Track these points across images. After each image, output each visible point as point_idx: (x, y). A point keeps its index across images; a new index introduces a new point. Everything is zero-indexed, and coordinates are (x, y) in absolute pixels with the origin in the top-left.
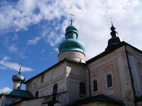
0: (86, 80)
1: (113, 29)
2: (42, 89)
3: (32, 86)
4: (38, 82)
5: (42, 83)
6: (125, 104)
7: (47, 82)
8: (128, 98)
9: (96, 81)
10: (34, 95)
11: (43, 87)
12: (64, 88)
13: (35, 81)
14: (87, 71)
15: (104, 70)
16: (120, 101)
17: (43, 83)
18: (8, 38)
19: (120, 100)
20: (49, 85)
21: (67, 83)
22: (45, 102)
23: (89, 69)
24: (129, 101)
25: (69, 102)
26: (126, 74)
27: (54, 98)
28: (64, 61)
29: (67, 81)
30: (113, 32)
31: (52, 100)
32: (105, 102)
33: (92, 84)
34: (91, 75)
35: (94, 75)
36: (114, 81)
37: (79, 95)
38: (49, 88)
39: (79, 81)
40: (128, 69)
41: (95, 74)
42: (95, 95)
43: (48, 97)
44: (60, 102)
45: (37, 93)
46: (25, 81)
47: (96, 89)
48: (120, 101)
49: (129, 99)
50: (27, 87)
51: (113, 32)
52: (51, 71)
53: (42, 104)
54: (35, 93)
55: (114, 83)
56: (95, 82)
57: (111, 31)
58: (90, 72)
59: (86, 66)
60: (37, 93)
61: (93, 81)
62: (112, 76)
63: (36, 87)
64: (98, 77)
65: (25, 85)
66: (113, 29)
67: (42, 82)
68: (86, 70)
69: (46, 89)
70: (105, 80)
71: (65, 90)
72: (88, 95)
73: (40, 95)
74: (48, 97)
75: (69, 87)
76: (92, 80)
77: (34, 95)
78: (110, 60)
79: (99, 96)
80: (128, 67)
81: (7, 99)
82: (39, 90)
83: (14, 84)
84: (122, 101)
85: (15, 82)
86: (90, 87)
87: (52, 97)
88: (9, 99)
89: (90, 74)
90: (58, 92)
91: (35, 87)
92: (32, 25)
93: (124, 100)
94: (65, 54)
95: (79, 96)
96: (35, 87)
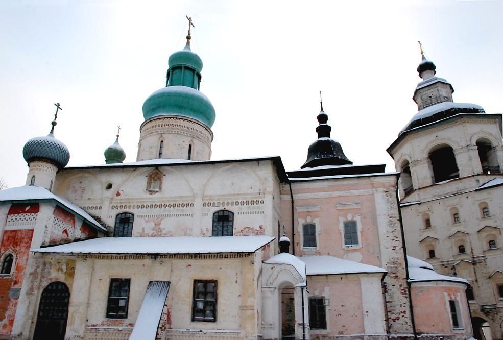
1: (323, 118)
6: (386, 283)
7: (181, 197)
14: (288, 197)
23: (295, 197)
24: (395, 278)
26: (392, 230)
30: (324, 130)
34: (298, 209)
35: (306, 210)
36: (362, 236)
40: (399, 221)
41: (310, 210)
46: (487, 234)
49: (397, 276)
51: (324, 130)
57: (317, 124)
62: (359, 227)
66: (323, 118)
76: (300, 224)
78: (355, 192)
80: (399, 218)
81: (56, 222)
85: (32, 164)
94: (169, 125)
96: (112, 199)
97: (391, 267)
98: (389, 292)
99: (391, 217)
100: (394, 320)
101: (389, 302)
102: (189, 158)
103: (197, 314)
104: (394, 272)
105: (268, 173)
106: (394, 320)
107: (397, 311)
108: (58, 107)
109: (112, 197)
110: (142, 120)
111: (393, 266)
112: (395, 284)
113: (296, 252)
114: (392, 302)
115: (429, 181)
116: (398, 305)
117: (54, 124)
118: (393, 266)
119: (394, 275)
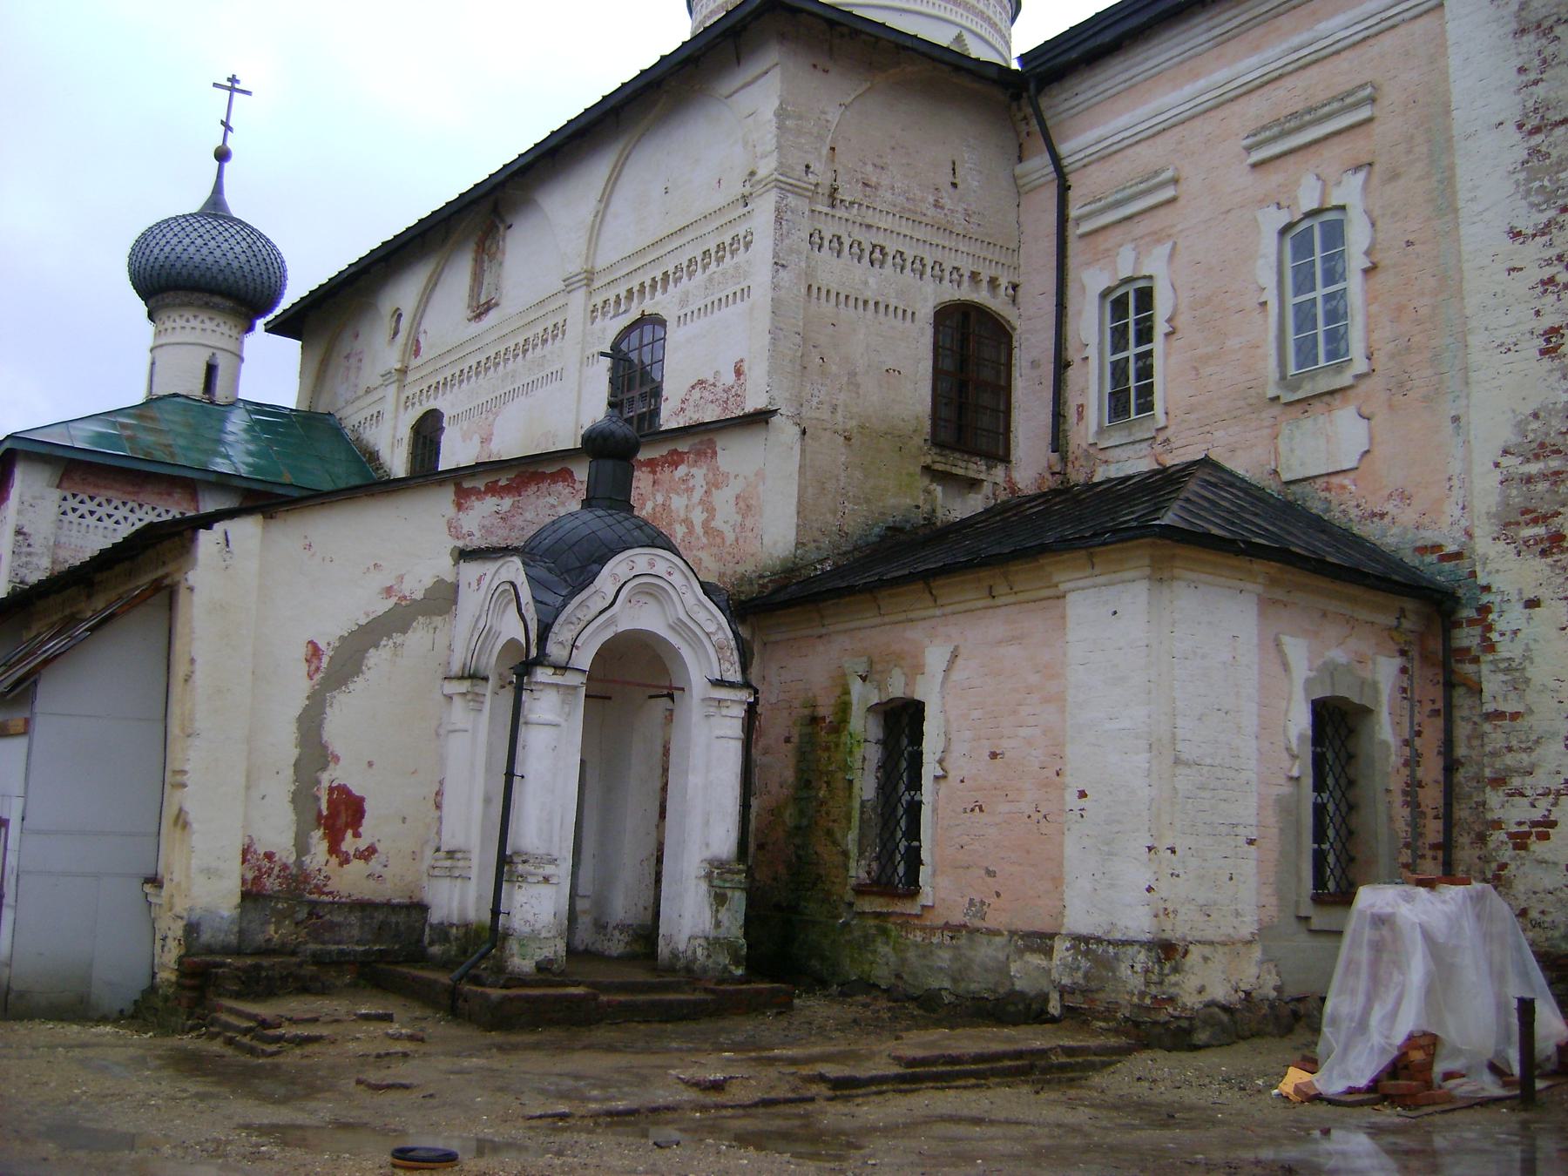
0: (1015, 287)
2: (483, 388)
3: (377, 349)
4: (436, 306)
5: (478, 317)
6: (1487, 589)
8: (1535, 521)
9: (1145, 298)
10: (397, 463)
11: (494, 362)
12: (738, 372)
13: (405, 293)
14: (1038, 165)
15: (1256, 156)
16: (1433, 558)
17: (492, 318)
18: (893, 959)
19: (1429, 536)
20: (558, 331)
21: (777, 308)
22: (495, 541)
23: (1064, 149)
24: (1544, 553)
25: (791, 536)
27: (611, 494)
28: (744, 28)
29: (775, 287)
31: (575, 506)
32: (1254, 551)
33: (1089, 326)
37: (928, 460)
38: (557, 375)
39: (929, 296)
42: (1114, 472)
43: (539, 478)
44: (678, 534)
45: (427, 432)
47: (1130, 395)
48: (1436, 548)
50: (318, 372)
52: (592, 177)
53: (464, 555)
54: (405, 433)
55: (1369, 331)
56: (1132, 308)
58: (1072, 180)
59: (1030, 110)
60: (427, 432)
61: (1104, 295)
62: (1357, 237)
63: (414, 363)
64: (1168, 246)
65: (294, 346)
67: (481, 310)
68: (1020, 159)
69: (529, 387)
70: (1262, 282)
71: (754, 402)
72: (1029, 463)
73: (455, 452)
74: (527, 472)
75: (802, 345)
76: (1092, 282)
77: (397, 463)
79: (1165, 482)
82: (445, 403)
83: (150, 328)
84: (1458, 556)
86: (1062, 365)
87: (581, 473)
88: (91, 505)
89: (1073, 212)
90: (669, 418)
91: (403, 371)
92: (1279, 594)
93: (1485, 545)
95: (927, 469)
96: (403, 371)
97: (1529, 479)
98: (1506, 649)
99: (1537, 130)
100: (1520, 841)
101: (1499, 715)
102: (486, 679)
103: (1118, 405)
104: (1544, 509)
105: (158, 352)
106: (1520, 841)
107: (1542, 779)
108: (232, 90)
109: (398, 366)
110: (195, 208)
111: (1534, 468)
112: (1540, 592)
113: (1334, 928)
114: (1515, 716)
115: (711, 570)
116: (1554, 735)
117: (222, 155)
118: (1534, 468)
119: (1540, 530)
